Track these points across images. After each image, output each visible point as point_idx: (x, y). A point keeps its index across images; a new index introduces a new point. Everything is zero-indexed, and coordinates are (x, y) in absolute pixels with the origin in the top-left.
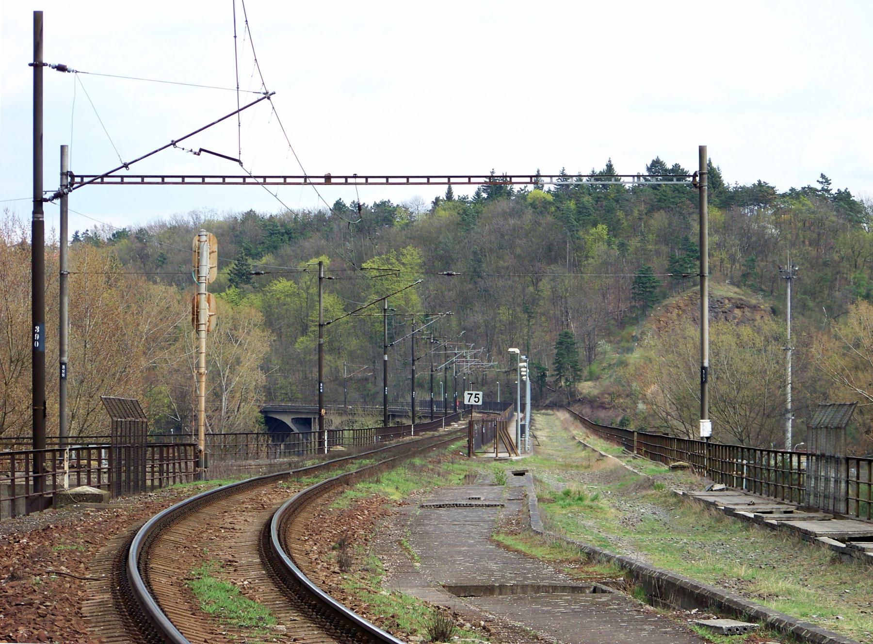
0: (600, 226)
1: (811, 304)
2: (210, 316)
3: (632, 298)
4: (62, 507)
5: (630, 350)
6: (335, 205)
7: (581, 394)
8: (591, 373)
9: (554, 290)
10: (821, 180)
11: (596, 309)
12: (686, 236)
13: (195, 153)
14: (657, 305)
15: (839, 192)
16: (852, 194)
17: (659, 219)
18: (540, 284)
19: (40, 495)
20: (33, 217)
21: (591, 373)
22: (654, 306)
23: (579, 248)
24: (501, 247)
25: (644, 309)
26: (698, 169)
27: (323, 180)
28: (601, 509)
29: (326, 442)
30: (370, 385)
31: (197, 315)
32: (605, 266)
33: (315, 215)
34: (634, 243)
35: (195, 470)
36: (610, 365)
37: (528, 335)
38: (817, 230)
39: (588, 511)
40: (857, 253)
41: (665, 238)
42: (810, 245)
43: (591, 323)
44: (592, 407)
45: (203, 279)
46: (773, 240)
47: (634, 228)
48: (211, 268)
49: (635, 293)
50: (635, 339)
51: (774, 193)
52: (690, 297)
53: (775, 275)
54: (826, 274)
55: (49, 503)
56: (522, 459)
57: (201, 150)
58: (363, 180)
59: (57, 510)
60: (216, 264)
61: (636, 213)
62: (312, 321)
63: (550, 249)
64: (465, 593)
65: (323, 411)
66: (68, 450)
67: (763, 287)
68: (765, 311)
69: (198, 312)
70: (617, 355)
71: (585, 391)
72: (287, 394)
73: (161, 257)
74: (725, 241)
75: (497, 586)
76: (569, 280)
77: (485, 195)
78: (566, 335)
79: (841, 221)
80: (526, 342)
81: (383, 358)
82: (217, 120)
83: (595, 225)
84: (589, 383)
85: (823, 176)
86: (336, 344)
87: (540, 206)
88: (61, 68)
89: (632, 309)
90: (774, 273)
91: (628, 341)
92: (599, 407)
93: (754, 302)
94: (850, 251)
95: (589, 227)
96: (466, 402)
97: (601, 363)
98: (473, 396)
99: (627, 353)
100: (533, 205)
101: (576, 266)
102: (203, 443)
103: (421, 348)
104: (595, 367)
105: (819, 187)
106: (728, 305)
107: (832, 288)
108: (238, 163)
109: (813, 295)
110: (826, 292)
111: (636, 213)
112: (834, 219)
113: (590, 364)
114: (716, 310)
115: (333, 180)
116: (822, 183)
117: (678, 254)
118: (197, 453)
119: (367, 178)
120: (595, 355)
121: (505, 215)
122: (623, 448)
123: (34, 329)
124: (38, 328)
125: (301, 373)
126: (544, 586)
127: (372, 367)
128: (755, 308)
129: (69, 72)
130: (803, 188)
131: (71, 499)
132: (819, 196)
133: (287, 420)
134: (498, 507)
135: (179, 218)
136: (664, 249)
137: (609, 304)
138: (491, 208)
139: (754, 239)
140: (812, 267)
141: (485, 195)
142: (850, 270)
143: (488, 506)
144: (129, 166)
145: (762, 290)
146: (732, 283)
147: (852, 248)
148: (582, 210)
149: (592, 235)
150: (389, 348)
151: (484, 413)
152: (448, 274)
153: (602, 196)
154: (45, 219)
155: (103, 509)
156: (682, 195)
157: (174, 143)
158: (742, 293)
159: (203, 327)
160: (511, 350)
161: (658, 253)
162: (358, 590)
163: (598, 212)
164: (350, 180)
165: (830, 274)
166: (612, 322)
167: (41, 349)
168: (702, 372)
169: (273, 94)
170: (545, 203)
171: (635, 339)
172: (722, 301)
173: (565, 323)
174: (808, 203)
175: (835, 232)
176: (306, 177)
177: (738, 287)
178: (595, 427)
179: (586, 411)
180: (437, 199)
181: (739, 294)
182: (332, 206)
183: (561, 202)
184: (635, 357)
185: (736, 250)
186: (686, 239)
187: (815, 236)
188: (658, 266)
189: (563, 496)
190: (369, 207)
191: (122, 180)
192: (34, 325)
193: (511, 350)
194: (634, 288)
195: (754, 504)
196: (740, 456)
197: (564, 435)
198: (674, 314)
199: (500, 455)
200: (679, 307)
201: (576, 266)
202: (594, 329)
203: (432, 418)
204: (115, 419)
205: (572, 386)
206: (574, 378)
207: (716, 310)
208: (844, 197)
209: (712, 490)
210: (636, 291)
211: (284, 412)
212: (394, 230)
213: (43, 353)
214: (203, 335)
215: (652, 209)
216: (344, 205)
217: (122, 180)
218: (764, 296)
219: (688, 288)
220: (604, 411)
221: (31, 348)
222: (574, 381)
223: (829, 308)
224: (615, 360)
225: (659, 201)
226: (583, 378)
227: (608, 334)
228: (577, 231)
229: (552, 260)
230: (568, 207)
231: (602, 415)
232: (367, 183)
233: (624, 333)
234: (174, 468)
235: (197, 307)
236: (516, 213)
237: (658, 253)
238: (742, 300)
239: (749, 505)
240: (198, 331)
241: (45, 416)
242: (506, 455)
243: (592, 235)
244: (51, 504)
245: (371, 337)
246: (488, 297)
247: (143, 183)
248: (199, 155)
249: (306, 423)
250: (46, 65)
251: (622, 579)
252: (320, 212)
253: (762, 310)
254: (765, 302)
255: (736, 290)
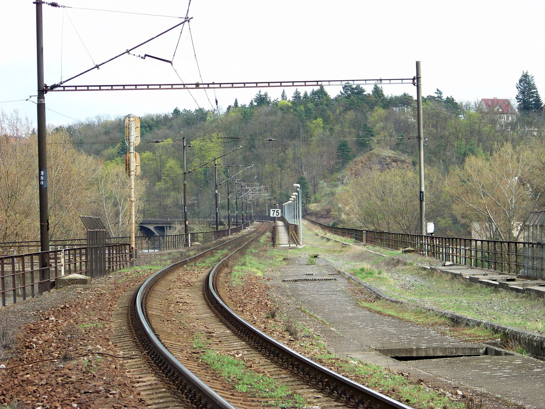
0: (318, 119)
1: (434, 159)
2: (137, 166)
3: (337, 158)
4: (61, 288)
5: (336, 186)
6: (174, 111)
7: (310, 210)
8: (315, 198)
9: (294, 154)
10: (437, 92)
11: (317, 164)
12: (366, 124)
13: (142, 58)
14: (350, 161)
15: (448, 98)
16: (455, 99)
17: (351, 115)
18: (287, 151)
19: (48, 281)
20: (38, 101)
21: (315, 198)
22: (349, 162)
23: (307, 132)
24: (266, 132)
25: (344, 164)
26: (416, 75)
27: (194, 86)
28: (386, 279)
29: (190, 240)
30: (196, 208)
31: (129, 166)
32: (322, 141)
33: (163, 117)
34: (337, 128)
35: (130, 260)
36: (326, 194)
37: (281, 179)
38: (436, 119)
39: (378, 281)
40: (458, 131)
41: (354, 124)
42: (433, 127)
43: (315, 172)
44: (317, 217)
45: (132, 144)
46: (413, 125)
47: (337, 120)
48: (136, 137)
49: (338, 155)
50: (338, 180)
51: (412, 100)
52: (368, 156)
53: (414, 144)
54: (442, 143)
55: (53, 285)
56: (303, 248)
57: (146, 55)
58: (218, 86)
59: (59, 290)
60: (139, 135)
61: (338, 111)
62: (163, 174)
63: (291, 132)
64: (391, 354)
65: (187, 222)
66: (63, 251)
67: (408, 150)
68: (409, 163)
69: (129, 164)
70: (330, 189)
71: (313, 209)
72: (151, 214)
73: (80, 141)
74: (386, 126)
75: (415, 349)
76: (303, 149)
77: (255, 104)
78: (302, 178)
79: (449, 114)
80: (279, 182)
81: (215, 192)
82: (156, 36)
83: (316, 118)
84: (315, 204)
85: (438, 90)
86: (177, 186)
87: (285, 109)
88: (54, 5)
89: (337, 163)
90: (413, 142)
91: (335, 181)
92: (320, 217)
93: (403, 158)
94: (454, 130)
95: (312, 120)
96: (271, 215)
97: (321, 193)
98: (276, 212)
99: (335, 187)
100: (282, 109)
101: (306, 141)
102: (134, 243)
103: (223, 187)
104: (317, 195)
105: (436, 95)
106: (389, 161)
107: (445, 150)
108: (170, 64)
109: (435, 154)
110: (442, 153)
111: (338, 111)
112: (445, 112)
113: (315, 194)
114: (382, 163)
115: (201, 86)
116: (437, 93)
117: (361, 133)
118: (131, 249)
119: (220, 84)
120: (317, 189)
121: (267, 114)
122: (354, 240)
123: (40, 173)
124: (42, 173)
125: (158, 202)
126: (449, 348)
127: (196, 198)
128: (403, 162)
129: (59, 7)
130: (428, 96)
131: (66, 282)
132: (436, 100)
133: (151, 228)
134: (334, 281)
135: (90, 120)
136: (353, 130)
137: (324, 161)
138: (259, 110)
139: (402, 125)
140: (434, 139)
141: (255, 104)
142: (455, 140)
143: (326, 280)
144: (99, 67)
145: (407, 152)
146: (391, 149)
147: (456, 128)
148: (308, 111)
149: (314, 124)
150: (219, 186)
151: (259, 221)
152: (269, 140)
153: (319, 103)
154: (46, 102)
155: (88, 289)
156: (363, 101)
157: (128, 52)
158: (396, 153)
159: (132, 173)
160: (295, 185)
161: (350, 133)
162: (334, 361)
163: (317, 112)
164: (210, 86)
165: (444, 142)
166: (326, 171)
167: (45, 186)
168: (420, 194)
169: (191, 18)
170: (288, 108)
171: (338, 180)
172: (386, 158)
173: (301, 172)
174: (430, 104)
175: (446, 120)
176: (184, 85)
177: (394, 150)
178: (324, 227)
179: (314, 219)
180: (230, 107)
181: (394, 154)
182: (172, 112)
183: (296, 107)
184: (339, 189)
185: (392, 131)
186: (366, 125)
187: (435, 122)
188: (351, 139)
189: (360, 272)
190: (193, 112)
191: (76, 89)
192: (40, 170)
193: (295, 185)
194: (337, 152)
195: (487, 275)
196: (463, 244)
197: (311, 233)
198: (360, 166)
199: (291, 245)
200: (362, 162)
201: (306, 141)
202: (317, 175)
203: (237, 225)
204: (89, 230)
205: (305, 206)
206: (306, 201)
207: (382, 163)
208: (450, 101)
209: (445, 266)
210: (339, 154)
211: (149, 223)
212: (207, 123)
213: (46, 188)
214: (133, 177)
215: (347, 109)
216: (179, 111)
217: (76, 89)
218: (408, 155)
219: (367, 151)
220: (323, 219)
221: (38, 186)
222: (307, 203)
223: (443, 161)
224: (328, 192)
225: (350, 105)
226: (311, 201)
227: (324, 177)
228: (306, 122)
229: (294, 138)
230: (301, 110)
231: (322, 221)
232: (220, 87)
233: (333, 176)
234: (120, 259)
235: (129, 161)
236: (273, 113)
237: (350, 133)
238: (396, 157)
239: (484, 275)
240: (129, 175)
241: (48, 229)
242: (294, 245)
243: (314, 124)
244: (54, 285)
245: (196, 182)
246: (258, 158)
247: (88, 90)
248: (144, 58)
249: (161, 229)
250: (43, 3)
251: (499, 340)
252: (166, 115)
253: (407, 163)
254: (409, 158)
255: (393, 152)
